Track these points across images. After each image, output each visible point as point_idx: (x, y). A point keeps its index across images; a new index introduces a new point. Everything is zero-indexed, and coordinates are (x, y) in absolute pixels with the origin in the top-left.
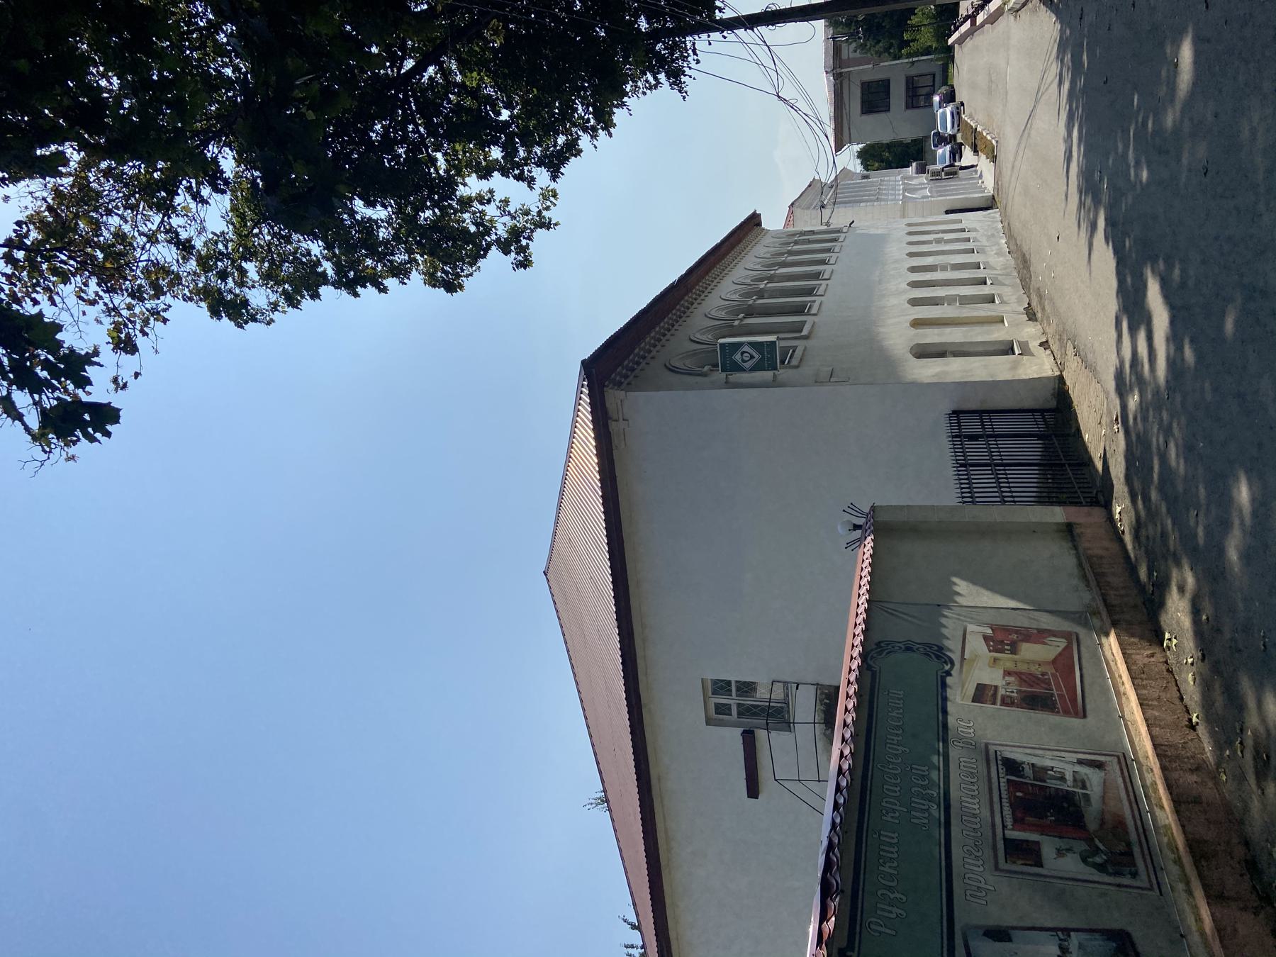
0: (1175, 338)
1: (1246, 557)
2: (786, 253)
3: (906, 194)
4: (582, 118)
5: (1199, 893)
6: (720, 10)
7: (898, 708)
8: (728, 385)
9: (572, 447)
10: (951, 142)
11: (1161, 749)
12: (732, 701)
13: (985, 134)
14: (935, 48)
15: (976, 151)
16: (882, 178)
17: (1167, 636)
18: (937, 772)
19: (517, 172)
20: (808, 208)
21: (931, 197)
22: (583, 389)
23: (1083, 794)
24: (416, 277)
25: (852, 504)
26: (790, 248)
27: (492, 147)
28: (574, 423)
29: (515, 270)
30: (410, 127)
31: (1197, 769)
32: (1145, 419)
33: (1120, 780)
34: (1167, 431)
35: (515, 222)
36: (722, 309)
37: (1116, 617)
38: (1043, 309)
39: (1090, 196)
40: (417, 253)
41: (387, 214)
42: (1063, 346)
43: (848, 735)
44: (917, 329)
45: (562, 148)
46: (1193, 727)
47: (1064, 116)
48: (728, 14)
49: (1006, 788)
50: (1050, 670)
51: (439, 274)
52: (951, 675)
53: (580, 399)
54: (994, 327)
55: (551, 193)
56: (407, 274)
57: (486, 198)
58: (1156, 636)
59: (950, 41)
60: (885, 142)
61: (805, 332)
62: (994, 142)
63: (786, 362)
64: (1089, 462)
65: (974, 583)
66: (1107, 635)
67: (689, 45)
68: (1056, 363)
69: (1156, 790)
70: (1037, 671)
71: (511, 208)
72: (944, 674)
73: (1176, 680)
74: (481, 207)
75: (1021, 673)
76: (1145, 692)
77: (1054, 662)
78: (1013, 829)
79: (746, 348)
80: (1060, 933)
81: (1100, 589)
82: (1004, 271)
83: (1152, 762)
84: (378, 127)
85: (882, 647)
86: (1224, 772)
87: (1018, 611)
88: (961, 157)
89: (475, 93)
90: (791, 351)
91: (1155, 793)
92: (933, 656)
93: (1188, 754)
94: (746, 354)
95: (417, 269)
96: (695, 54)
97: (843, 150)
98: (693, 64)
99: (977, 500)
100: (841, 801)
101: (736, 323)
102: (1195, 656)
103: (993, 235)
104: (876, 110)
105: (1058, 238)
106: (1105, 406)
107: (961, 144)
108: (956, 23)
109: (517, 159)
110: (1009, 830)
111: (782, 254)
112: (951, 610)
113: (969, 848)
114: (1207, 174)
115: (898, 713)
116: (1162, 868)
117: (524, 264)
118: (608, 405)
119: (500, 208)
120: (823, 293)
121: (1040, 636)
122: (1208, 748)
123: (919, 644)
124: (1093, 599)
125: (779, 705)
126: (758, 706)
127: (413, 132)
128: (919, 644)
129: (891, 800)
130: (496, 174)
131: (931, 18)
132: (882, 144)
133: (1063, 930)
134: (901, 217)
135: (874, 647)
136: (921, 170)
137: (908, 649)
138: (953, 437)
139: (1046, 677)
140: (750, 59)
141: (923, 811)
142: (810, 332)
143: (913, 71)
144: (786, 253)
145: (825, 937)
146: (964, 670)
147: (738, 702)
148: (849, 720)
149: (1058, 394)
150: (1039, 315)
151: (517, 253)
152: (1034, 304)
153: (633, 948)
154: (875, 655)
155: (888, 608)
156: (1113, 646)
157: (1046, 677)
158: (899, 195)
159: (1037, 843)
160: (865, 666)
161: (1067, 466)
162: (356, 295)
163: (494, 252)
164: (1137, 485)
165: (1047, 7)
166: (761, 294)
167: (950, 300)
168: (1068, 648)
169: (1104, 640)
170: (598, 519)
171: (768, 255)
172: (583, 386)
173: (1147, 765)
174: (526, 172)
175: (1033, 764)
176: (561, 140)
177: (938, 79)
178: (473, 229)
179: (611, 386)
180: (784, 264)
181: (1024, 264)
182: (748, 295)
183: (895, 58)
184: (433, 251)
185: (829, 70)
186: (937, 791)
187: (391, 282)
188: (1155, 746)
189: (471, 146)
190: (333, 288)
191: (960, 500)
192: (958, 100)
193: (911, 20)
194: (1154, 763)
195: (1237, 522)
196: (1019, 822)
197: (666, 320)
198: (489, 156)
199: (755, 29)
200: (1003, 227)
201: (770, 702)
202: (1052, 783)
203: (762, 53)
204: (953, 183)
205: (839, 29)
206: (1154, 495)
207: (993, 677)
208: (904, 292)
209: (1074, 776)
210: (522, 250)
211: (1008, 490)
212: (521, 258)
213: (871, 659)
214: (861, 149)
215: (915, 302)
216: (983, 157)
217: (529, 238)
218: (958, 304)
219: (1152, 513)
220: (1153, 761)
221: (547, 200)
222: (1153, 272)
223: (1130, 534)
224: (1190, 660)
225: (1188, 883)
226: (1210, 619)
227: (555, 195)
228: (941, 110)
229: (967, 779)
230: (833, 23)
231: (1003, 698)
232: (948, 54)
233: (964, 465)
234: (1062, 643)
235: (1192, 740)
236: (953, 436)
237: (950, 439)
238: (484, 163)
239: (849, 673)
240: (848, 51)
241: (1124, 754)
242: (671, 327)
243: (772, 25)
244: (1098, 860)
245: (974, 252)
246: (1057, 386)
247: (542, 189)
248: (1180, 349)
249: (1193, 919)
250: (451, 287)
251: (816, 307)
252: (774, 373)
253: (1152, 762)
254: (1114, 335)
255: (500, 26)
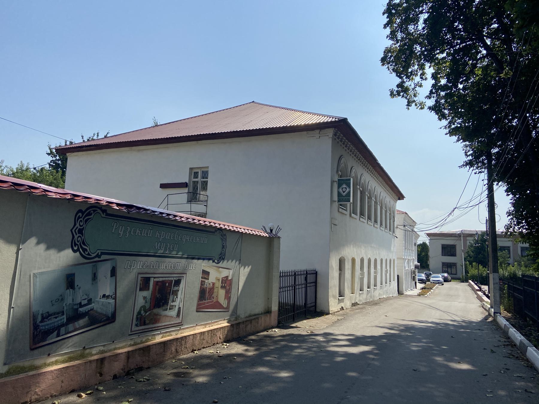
0: (346, 354)
1: (261, 373)
2: (386, 209)
3: (407, 260)
4: (455, 122)
5: (130, 349)
6: (497, 184)
7: (200, 241)
8: (332, 182)
9: (308, 114)
10: (427, 279)
11: (184, 339)
12: (199, 179)
13: (429, 292)
14: (468, 275)
15: (422, 289)
16: (414, 251)
17: (228, 344)
18: (175, 254)
19: (434, 91)
20: (404, 220)
21: (405, 270)
22: (334, 119)
23: (167, 308)
24: (389, 43)
25: (281, 229)
26: (388, 211)
27: (446, 80)
28: (320, 115)
29: (389, 90)
30: (459, 41)
31: (177, 351)
32: (313, 342)
33: (173, 323)
34: (309, 349)
35: (411, 90)
36: (364, 181)
37: (235, 326)
38: (357, 309)
39: (404, 328)
40: (400, 43)
41: (420, 29)
42: (341, 315)
43: (189, 220)
44: (351, 260)
45: (443, 112)
46: (193, 351)
47: (438, 321)
48: (495, 187)
49: (170, 280)
50: (215, 300)
51: (390, 54)
52: (213, 262)
53: (330, 117)
54: (350, 291)
55: (423, 106)
56: (391, 39)
57: (423, 77)
58: (228, 340)
59: (470, 281)
60: (429, 253)
61: (353, 215)
62: (426, 296)
63: (341, 206)
64: (294, 321)
65: (249, 274)
66: (228, 322)
67: (483, 170)
68: (335, 312)
69: (169, 336)
70: (214, 295)
71: (418, 88)
72: (213, 260)
73: (211, 346)
74: (419, 74)
75: (213, 289)
76: (206, 334)
77: (218, 302)
78: (154, 281)
79: (348, 190)
80: (114, 296)
81: (245, 321)
82: (373, 296)
83: (180, 335)
84: (460, 27)
85: (224, 236)
86: (176, 361)
87: (237, 290)
88: (420, 283)
89: (472, 72)
90: (345, 209)
91: (168, 335)
92: (220, 256)
93: (183, 349)
94: (345, 189)
95: (393, 44)
96: (479, 172)
97: (427, 236)
98: (474, 171)
99: (281, 278)
100: (164, 215)
101: (358, 187)
102: (220, 354)
103: (387, 293)
104: (443, 252)
105: (386, 316)
106: (317, 329)
107: (425, 283)
108: (478, 284)
109: (440, 91)
110: (154, 280)
111: (386, 208)
112: (239, 264)
113: (146, 263)
114: (414, 371)
115: (198, 240)
116: (139, 336)
117: (392, 94)
118: (327, 129)
119: (418, 83)
120: (368, 223)
121: (228, 297)
122: (185, 356)
123: (225, 251)
124: (241, 319)
125: (198, 198)
126: (197, 190)
127: (457, 42)
128: (225, 251)
129: (164, 235)
130: (434, 81)
131: (481, 274)
132: (428, 252)
133: (116, 297)
134: (397, 257)
135: (224, 233)
136: (416, 267)
137: (223, 247)
138: (307, 271)
139: (212, 298)
140: (474, 196)
141: (160, 247)
142: (353, 217)
143: (458, 266)
144: (386, 209)
145: (110, 205)
146: (215, 268)
147: (199, 181)
148: (195, 221)
149: (322, 312)
150: (354, 307)
151: (397, 91)
152: (359, 306)
153: (97, 136)
154: (221, 233)
155: (239, 241)
156: (224, 324)
157: (212, 298)
158: (407, 257)
159: (148, 289)
160: (217, 229)
161: (294, 313)
162: (384, 14)
163: (399, 80)
164: (287, 338)
165: (484, 318)
166: (370, 198)
167: (362, 274)
168: (223, 308)
169: (226, 321)
170: (277, 124)
171: (385, 202)
172: (336, 118)
173: (178, 333)
174: (433, 95)
175: (179, 291)
176: (446, 112)
177: (454, 276)
178: (410, 70)
179: (335, 131)
180: (381, 208)
181: (375, 303)
182: (370, 193)
183: (465, 259)
184: (401, 51)
185: (463, 232)
186: (168, 253)
187: (388, 31)
188: (185, 337)
189: (448, 70)
190: (388, 2)
191: (281, 272)
192: (445, 283)
193: (481, 265)
194: (179, 336)
195: (273, 371)
196: (157, 283)
197: (362, 157)
198: (442, 79)
199: (487, 199)
200: (390, 297)
201: (199, 194)
202: (171, 297)
203: (476, 201)
204: (410, 279)
205: (480, 237)
206: (283, 343)
207: (212, 279)
208: (367, 256)
209: (174, 305)
210: (398, 94)
211: (285, 290)
212: (394, 93)
213: (219, 232)
214: (427, 244)
215: (362, 260)
216: (420, 291)
217: (403, 96)
218: (360, 277)
219: (276, 342)
220: (180, 335)
221: (420, 104)
222: (373, 349)
223: (267, 334)
224: (218, 352)
225: (133, 345)
226: (235, 360)
227: (421, 108)
228: (441, 276)
229: (173, 265)
230: (483, 234)
231: (204, 281)
232: (464, 280)
233: (295, 274)
234: (225, 305)
235: (188, 351)
236: (307, 271)
237: (306, 270)
238: (439, 76)
239: (214, 223)
240: (470, 240)
241: (183, 325)
242: (358, 159)
243: (488, 206)
244: (142, 312)
245: (381, 285)
246: (325, 312)
247: (425, 102)
248: (342, 356)
249: (120, 346)
250: (384, 60)
251: (363, 220)
252: (336, 201)
253: (180, 335)
254: (346, 333)
255: (509, 76)
